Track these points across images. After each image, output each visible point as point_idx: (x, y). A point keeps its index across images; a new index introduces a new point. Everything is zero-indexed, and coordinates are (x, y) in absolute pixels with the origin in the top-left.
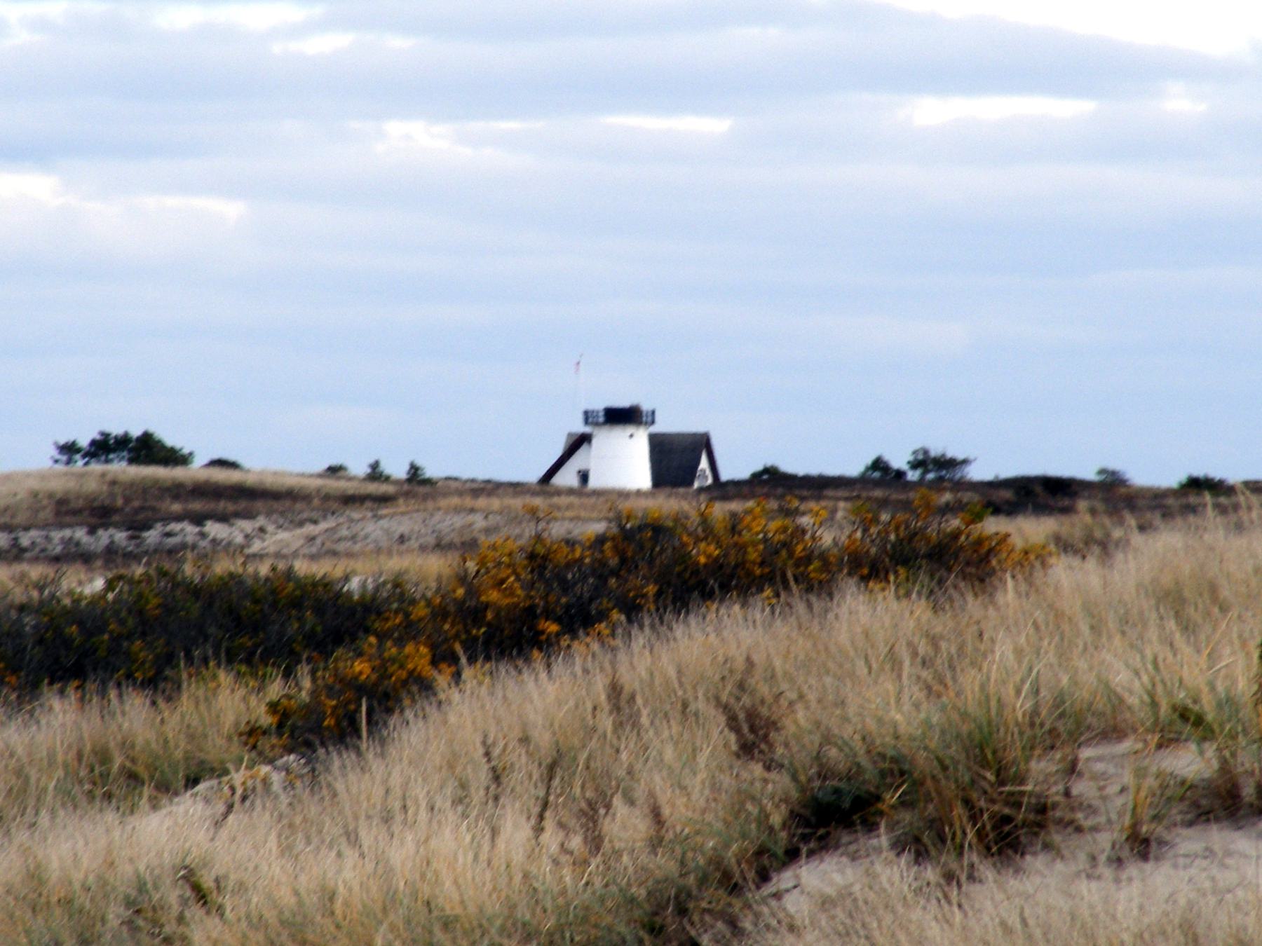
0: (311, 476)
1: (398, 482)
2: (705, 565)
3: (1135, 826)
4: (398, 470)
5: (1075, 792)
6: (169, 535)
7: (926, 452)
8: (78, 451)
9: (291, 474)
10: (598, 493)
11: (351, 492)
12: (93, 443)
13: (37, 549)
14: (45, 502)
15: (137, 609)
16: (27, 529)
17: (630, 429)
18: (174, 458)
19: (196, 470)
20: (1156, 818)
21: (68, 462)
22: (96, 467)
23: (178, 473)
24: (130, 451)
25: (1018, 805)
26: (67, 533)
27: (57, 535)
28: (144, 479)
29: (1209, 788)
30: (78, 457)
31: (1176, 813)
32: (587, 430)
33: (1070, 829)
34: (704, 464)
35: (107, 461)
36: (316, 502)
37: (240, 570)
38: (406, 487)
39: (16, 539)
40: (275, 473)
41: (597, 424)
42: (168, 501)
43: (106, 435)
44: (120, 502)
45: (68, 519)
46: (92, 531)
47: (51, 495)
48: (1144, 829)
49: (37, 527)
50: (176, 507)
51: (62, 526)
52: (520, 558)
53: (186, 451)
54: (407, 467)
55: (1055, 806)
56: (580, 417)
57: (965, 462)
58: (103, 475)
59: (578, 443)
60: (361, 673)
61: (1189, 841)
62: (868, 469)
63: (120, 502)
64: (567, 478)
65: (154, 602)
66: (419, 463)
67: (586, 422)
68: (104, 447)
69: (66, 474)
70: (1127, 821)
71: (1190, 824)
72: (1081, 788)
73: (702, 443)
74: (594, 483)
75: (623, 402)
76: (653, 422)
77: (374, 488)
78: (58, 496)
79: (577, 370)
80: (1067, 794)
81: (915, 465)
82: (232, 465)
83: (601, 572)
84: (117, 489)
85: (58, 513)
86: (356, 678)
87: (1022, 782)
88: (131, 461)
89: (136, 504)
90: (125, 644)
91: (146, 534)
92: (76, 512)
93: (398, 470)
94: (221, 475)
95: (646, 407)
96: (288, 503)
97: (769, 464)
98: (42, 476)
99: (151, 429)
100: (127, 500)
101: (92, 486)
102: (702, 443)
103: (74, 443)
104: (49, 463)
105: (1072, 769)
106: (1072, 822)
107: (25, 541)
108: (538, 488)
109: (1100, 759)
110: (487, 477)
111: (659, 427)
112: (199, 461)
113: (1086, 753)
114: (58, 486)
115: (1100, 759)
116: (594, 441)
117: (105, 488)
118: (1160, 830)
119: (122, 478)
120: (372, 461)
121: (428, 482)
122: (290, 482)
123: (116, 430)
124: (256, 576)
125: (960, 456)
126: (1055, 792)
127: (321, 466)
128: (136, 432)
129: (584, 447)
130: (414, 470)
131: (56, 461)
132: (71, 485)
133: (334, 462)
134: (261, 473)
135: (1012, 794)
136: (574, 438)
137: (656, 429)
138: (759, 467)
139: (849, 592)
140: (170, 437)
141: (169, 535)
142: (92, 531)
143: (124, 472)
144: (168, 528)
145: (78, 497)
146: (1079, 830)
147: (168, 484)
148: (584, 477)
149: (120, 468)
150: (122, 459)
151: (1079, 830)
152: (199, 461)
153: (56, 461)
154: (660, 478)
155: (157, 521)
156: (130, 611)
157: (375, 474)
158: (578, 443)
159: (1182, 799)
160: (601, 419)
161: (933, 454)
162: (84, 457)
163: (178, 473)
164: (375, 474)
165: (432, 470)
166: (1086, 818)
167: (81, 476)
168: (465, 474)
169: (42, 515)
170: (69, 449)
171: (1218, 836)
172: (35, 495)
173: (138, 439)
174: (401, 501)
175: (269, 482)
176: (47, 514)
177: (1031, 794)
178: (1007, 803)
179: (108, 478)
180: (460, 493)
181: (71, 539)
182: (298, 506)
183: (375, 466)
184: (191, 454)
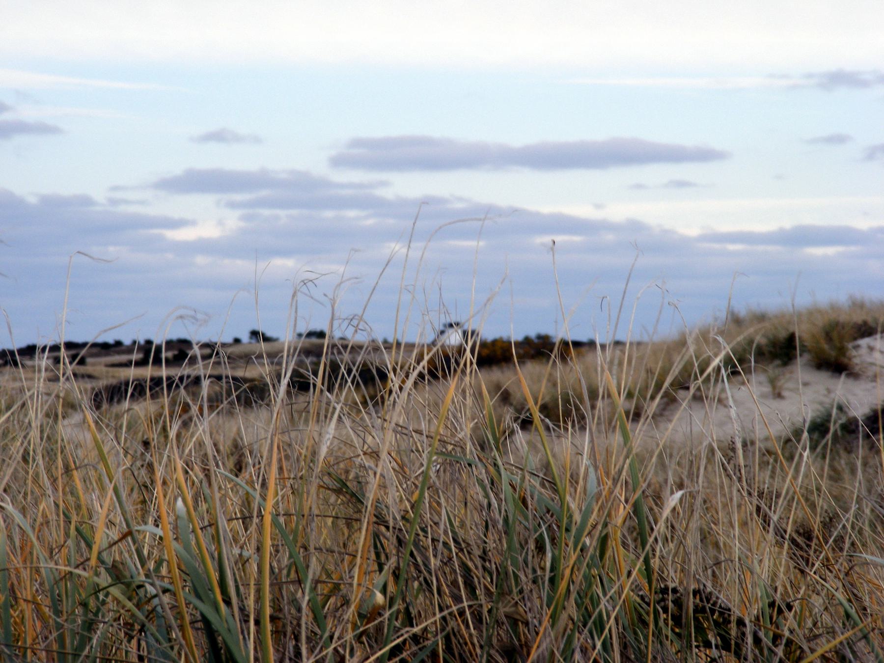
59: (442, 332)
68: (310, 334)
138: (532, 333)
165: (742, 312)
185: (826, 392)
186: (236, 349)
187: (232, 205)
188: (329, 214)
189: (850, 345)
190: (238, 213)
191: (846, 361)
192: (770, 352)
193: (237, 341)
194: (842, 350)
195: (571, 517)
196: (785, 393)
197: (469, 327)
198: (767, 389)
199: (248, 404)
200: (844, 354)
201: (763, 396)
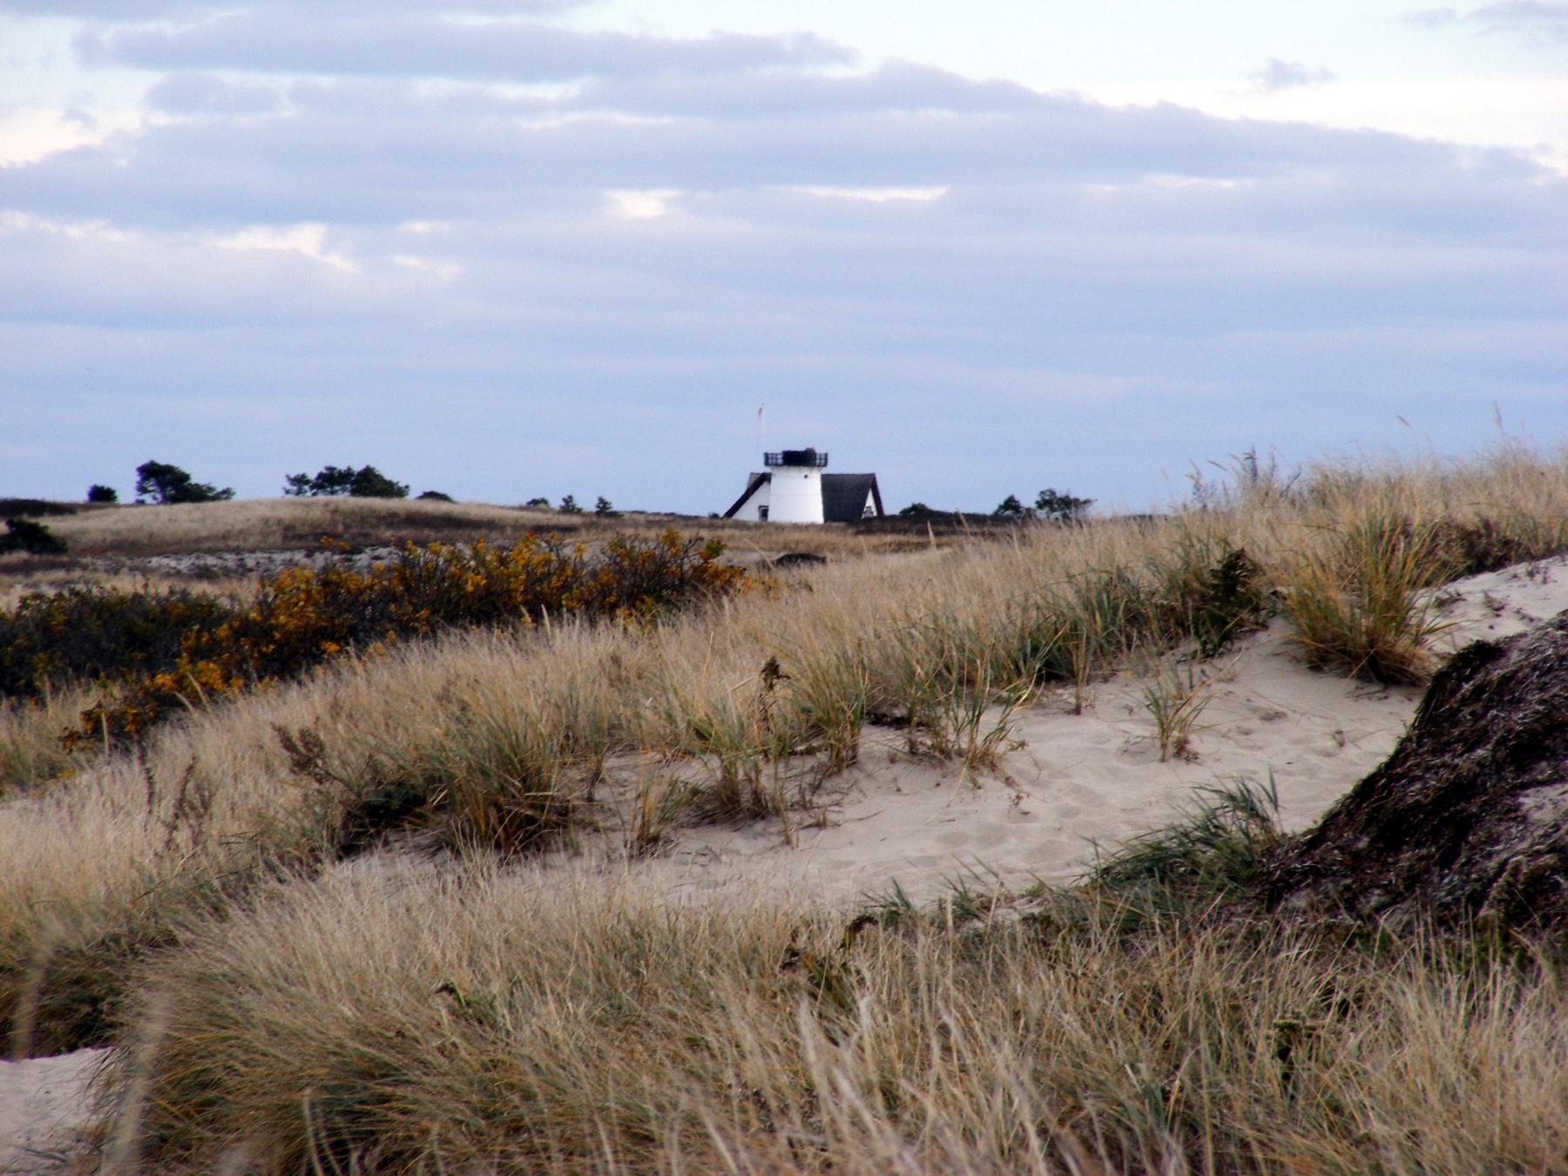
0: (513, 508)
1: (589, 515)
2: (472, 593)
3: (645, 825)
4: (588, 504)
5: (597, 797)
6: (377, 558)
7: (1053, 493)
8: (307, 482)
9: (493, 507)
10: (780, 528)
11: (544, 522)
12: (321, 476)
13: (261, 569)
14: (275, 528)
15: (44, 625)
16: (252, 551)
17: (805, 471)
18: (391, 490)
19: (410, 502)
20: (663, 820)
21: (299, 492)
22: (322, 497)
23: (393, 504)
24: (353, 483)
25: (542, 808)
26: (288, 555)
27: (279, 557)
28: (361, 508)
29: (715, 794)
30: (306, 487)
31: (682, 816)
32: (767, 470)
33: (589, 830)
34: (870, 502)
35: (333, 493)
36: (509, 531)
37: (141, 591)
38: (594, 519)
39: (242, 560)
40: (480, 505)
41: (777, 465)
42: (383, 529)
43: (331, 469)
44: (340, 528)
45: (294, 543)
46: (309, 555)
47: (280, 522)
48: (652, 830)
49: (263, 550)
50: (388, 534)
51: (284, 549)
52: (315, 587)
53: (402, 485)
54: (596, 502)
55: (575, 809)
56: (762, 460)
57: (1087, 502)
58: (326, 505)
59: (761, 480)
60: (163, 685)
61: (692, 842)
62: (1001, 507)
63: (340, 528)
64: (749, 513)
65: (61, 618)
66: (607, 498)
67: (767, 464)
68: (331, 479)
69: (293, 503)
70: (638, 823)
71: (695, 826)
72: (601, 793)
73: (869, 483)
74: (773, 516)
75: (799, 447)
76: (825, 465)
77: (565, 520)
78: (287, 523)
79: (760, 418)
80: (590, 799)
81: (1041, 505)
82: (444, 498)
83: (388, 596)
84: (338, 517)
85: (285, 537)
86: (159, 690)
87: (547, 787)
88: (354, 493)
89: (354, 531)
90: (28, 656)
91: (357, 557)
92: (301, 537)
93: (588, 504)
94: (431, 506)
95: (819, 450)
96: (484, 531)
97: (916, 502)
98: (273, 505)
99: (372, 466)
100: (347, 527)
101: (317, 514)
102: (869, 483)
103: (304, 476)
104: (282, 493)
105: (596, 777)
106: (591, 824)
107: (250, 561)
108: (707, 522)
109: (621, 768)
110: (669, 511)
111: (832, 469)
112: (414, 493)
113: (610, 762)
114: (286, 514)
115: (621, 768)
116: (773, 480)
117: (328, 515)
118: (667, 830)
119: (343, 507)
120: (566, 496)
121: (615, 515)
122: (493, 514)
123: (341, 466)
124: (156, 597)
125: (1082, 498)
126: (576, 797)
127: (524, 501)
128: (358, 467)
129: (765, 484)
130: (603, 506)
131: (287, 492)
132: (299, 513)
133: (537, 496)
134: (468, 504)
135: (535, 798)
136: (754, 480)
137: (826, 471)
138: (908, 505)
139: (602, 623)
140: (388, 473)
141: (377, 558)
142: (309, 555)
143: (345, 502)
144: (377, 553)
145: (303, 525)
146: (597, 830)
147: (383, 514)
148: (764, 512)
149: (344, 499)
150: (344, 490)
151: (597, 830)
152: (414, 493)
153: (287, 492)
154: (831, 513)
155: (366, 546)
156: (37, 626)
157: (569, 507)
158: (761, 480)
159: (688, 803)
160: (780, 461)
161: (1059, 494)
162: (312, 488)
163: (393, 504)
164: (569, 507)
165: (617, 506)
166: (606, 820)
167: (308, 505)
168: (650, 509)
169: (271, 539)
170: (300, 481)
171: (720, 838)
172: (266, 521)
173: (360, 474)
174: (583, 531)
175: (474, 513)
176: (276, 539)
177: (553, 798)
178: (532, 806)
179: (332, 507)
180: (636, 525)
181: (291, 560)
182: (493, 535)
183: (568, 500)
184: (407, 487)
185: (1330, 744)
186: (99, 524)
187: (137, 55)
188: (430, 87)
189: (1423, 598)
190: (151, 78)
191: (1403, 644)
192: (1167, 612)
193: (102, 496)
194: (1394, 612)
195: (1171, 1130)
196: (1196, 744)
197: (842, 464)
198: (1143, 729)
199: (1311, 668)
200: (1402, 627)
201: (1131, 751)
